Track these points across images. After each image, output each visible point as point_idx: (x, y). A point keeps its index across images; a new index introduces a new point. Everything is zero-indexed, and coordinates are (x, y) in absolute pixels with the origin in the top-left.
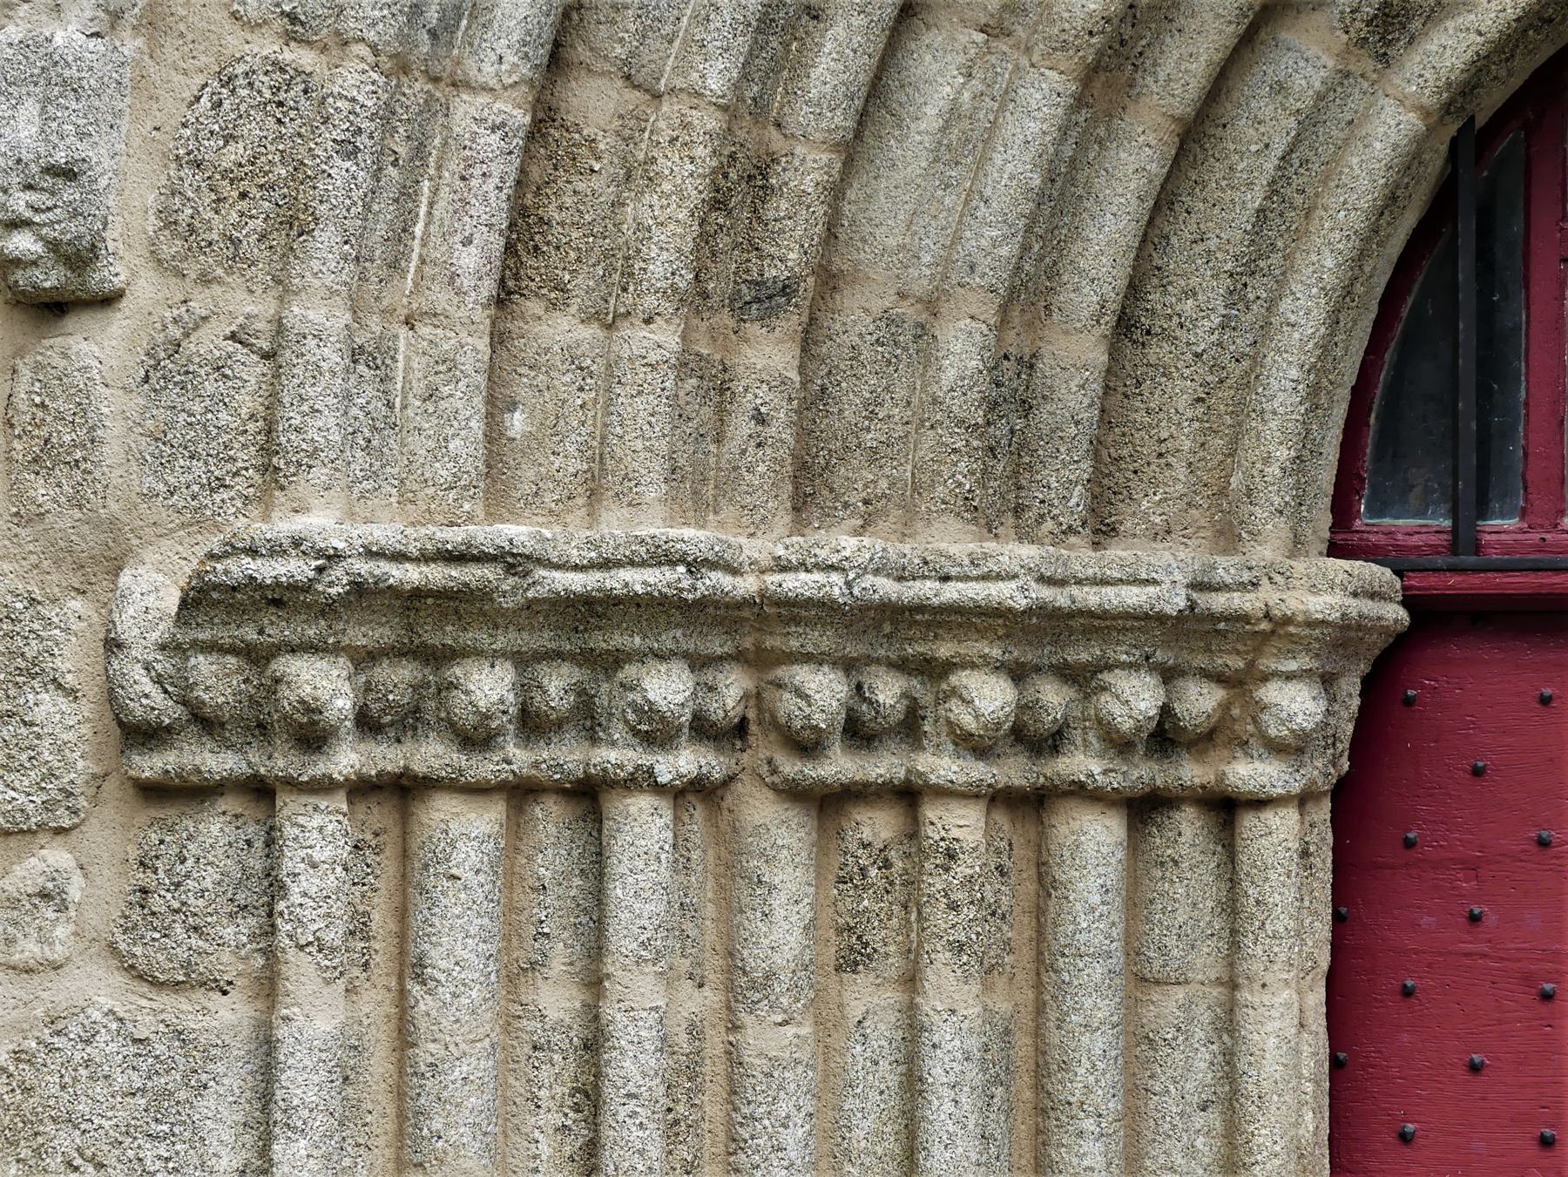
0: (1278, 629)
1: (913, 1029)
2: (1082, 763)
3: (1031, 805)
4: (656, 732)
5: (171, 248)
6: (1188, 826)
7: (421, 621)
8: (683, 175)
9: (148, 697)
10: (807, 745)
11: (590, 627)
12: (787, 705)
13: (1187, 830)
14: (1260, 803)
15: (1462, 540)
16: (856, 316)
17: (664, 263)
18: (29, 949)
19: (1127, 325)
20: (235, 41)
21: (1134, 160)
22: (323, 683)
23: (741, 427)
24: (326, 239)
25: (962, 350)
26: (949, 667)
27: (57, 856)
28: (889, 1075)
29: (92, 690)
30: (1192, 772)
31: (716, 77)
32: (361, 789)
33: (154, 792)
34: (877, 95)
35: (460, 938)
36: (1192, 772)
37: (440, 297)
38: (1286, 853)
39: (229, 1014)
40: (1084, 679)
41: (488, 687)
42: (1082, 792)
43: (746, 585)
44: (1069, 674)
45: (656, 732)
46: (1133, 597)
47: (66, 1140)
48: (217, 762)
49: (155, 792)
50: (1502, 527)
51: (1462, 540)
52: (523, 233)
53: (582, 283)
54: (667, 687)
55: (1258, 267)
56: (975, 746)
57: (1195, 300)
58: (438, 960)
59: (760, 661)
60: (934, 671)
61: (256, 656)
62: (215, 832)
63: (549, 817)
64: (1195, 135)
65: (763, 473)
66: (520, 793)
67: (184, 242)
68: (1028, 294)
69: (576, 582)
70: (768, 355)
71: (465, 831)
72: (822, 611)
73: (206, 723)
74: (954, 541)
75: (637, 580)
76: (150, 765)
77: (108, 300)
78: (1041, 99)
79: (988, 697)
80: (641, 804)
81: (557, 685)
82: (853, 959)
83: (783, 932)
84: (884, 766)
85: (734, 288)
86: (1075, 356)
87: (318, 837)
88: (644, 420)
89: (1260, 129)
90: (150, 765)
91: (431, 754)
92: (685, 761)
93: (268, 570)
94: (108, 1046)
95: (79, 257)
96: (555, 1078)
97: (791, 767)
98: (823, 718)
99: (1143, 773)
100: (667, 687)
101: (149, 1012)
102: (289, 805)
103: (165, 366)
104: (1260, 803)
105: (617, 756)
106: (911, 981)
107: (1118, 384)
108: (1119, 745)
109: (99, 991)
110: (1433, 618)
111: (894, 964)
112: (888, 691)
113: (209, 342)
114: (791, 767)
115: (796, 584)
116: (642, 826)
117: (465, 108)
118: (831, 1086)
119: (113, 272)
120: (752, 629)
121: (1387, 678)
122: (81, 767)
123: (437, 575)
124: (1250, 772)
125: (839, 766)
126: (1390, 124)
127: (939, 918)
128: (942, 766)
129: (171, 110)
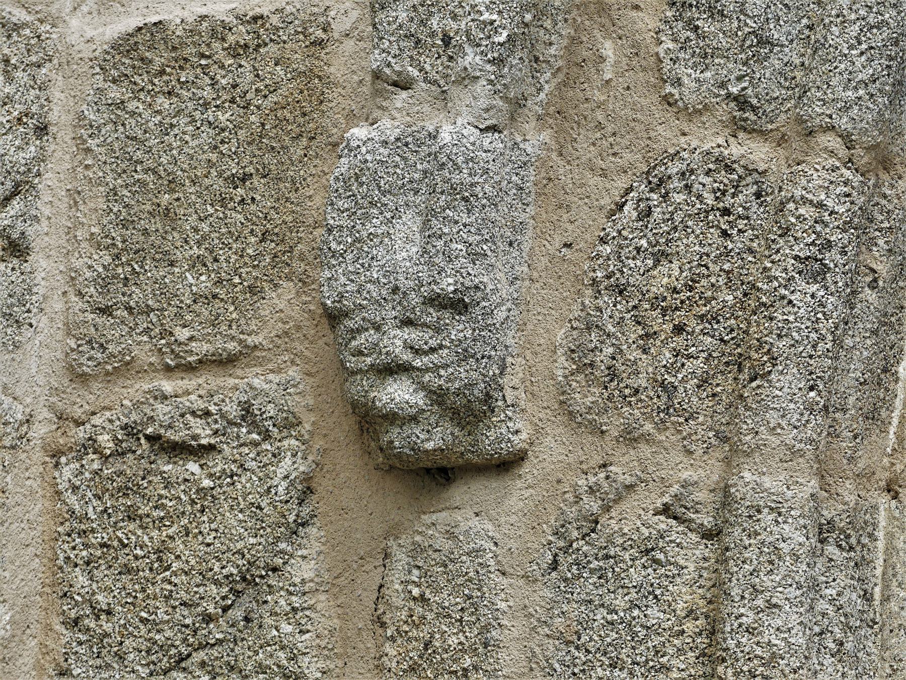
5: (586, 397)
20: (666, 133)
77: (506, 464)
95: (469, 410)
103: (575, 548)
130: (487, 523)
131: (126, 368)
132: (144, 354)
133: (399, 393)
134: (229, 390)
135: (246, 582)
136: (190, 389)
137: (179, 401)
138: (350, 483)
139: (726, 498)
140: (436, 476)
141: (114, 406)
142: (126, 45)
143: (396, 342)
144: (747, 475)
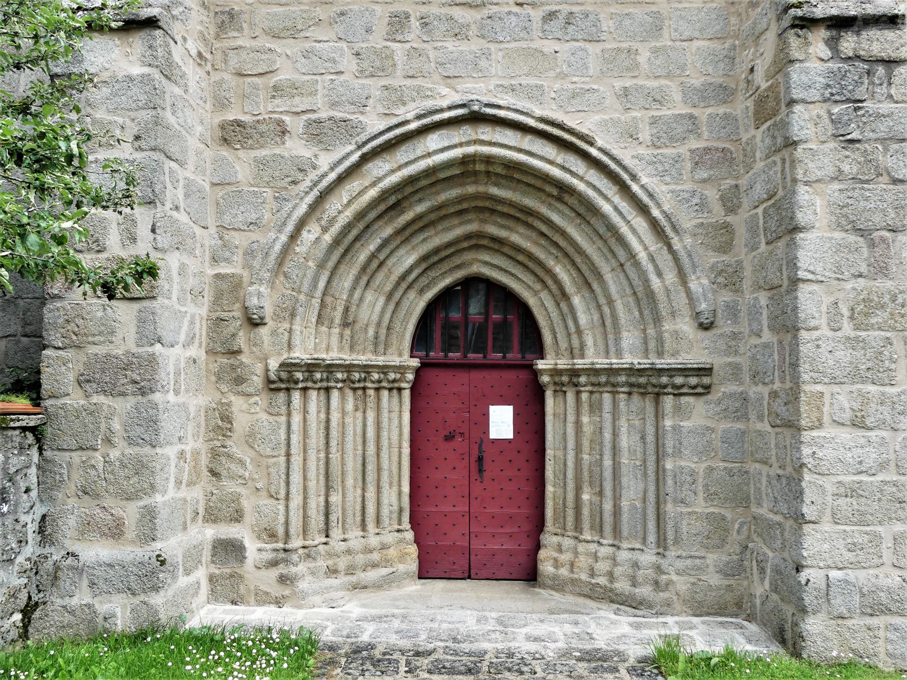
0: (408, 367)
1: (365, 418)
2: (384, 384)
3: (377, 389)
4: (337, 381)
5: (275, 318)
6: (395, 391)
7: (311, 368)
8: (340, 309)
9: (273, 377)
10: (353, 382)
11: (330, 368)
12: (352, 377)
13: (395, 391)
14: (404, 389)
15: (427, 355)
16: (357, 327)
17: (337, 321)
18: (253, 411)
19: (388, 328)
20: (284, 291)
21: (391, 307)
22: (299, 375)
23: (344, 341)
24: (298, 318)
25: (371, 332)
26: (333, 372)
27: (257, 398)
28: (361, 424)
29: (262, 376)
30: (396, 385)
31: (345, 297)
32: (301, 389)
33: (272, 390)
34: (361, 299)
35: (313, 407)
36: (396, 385)
37: (310, 325)
38: (407, 394)
39: (283, 419)
40: (385, 374)
41: (318, 376)
42: (384, 388)
43: (348, 362)
44: (383, 373)
45: (337, 381)
46: (393, 363)
47: (259, 436)
48: (283, 386)
49: (272, 390)
50: (432, 354)
51: (427, 355)
52: (319, 316)
53: (326, 323)
54: (339, 376)
55: (405, 321)
56: (373, 382)
57: (397, 326)
58: (310, 411)
59: (348, 372)
60: (368, 373)
61: (289, 372)
62: (282, 395)
63: (322, 392)
64: (398, 304)
65: (347, 347)
66: (319, 389)
67: (277, 317)
68: (379, 324)
69: (328, 362)
70: (348, 332)
71: (313, 394)
72: (359, 366)
73: (281, 380)
74: (370, 356)
75: (337, 362)
76: (273, 386)
77: (265, 324)
78: (382, 300)
79: (376, 376)
80: (335, 390)
81: (325, 375)
82: (356, 410)
83: (350, 406)
84: (361, 385)
85: (345, 324)
86: (383, 332)
87: (296, 396)
88: (335, 340)
89: (406, 304)
90: (273, 386)
91: (310, 384)
92: (340, 385)
93: (293, 361)
94: (265, 423)
95: (262, 318)
96: (322, 426)
97: (352, 385)
98: (358, 380)
99: (391, 385)
100: (339, 376)
101: (271, 419)
102: (292, 392)
103: (274, 333)
104: (404, 389)
105: (332, 384)
106: (364, 412)
107: (387, 335)
108: (389, 381)
109: (264, 416)
110: (424, 365)
111: (362, 410)
112: (363, 375)
113: (281, 330)
114: (352, 385)
115: (355, 362)
116: (335, 394)
117: (314, 300)
118: (355, 425)
119: (266, 320)
120: (349, 368)
121: (418, 371)
122: (261, 386)
123: (313, 361)
124: (404, 385)
125: (357, 385)
126: (421, 305)
127: (369, 404)
128: (369, 385)
129: (275, 299)
130: (263, 331)
131: (217, 311)
132: (219, 309)
133: (255, 316)
134: (231, 314)
135: (233, 335)
136: (226, 314)
137: (224, 315)
138: (246, 324)
139: (291, 329)
140: (257, 325)
141: (214, 316)
142: (216, 275)
143: (255, 311)
144: (845, 45)
